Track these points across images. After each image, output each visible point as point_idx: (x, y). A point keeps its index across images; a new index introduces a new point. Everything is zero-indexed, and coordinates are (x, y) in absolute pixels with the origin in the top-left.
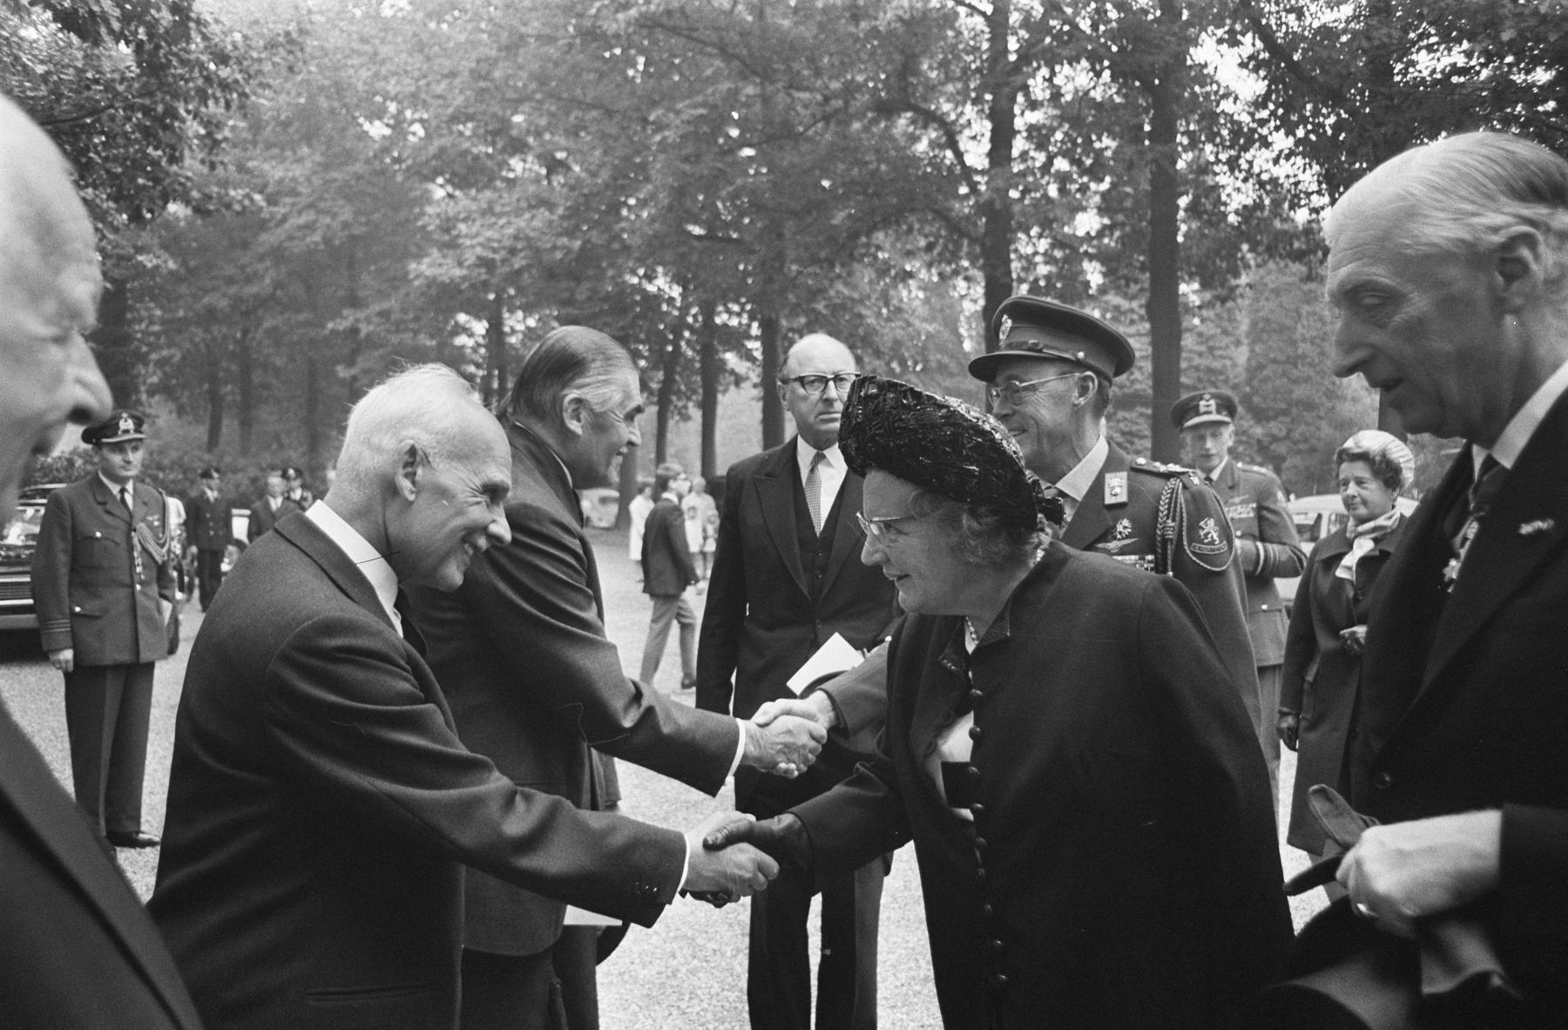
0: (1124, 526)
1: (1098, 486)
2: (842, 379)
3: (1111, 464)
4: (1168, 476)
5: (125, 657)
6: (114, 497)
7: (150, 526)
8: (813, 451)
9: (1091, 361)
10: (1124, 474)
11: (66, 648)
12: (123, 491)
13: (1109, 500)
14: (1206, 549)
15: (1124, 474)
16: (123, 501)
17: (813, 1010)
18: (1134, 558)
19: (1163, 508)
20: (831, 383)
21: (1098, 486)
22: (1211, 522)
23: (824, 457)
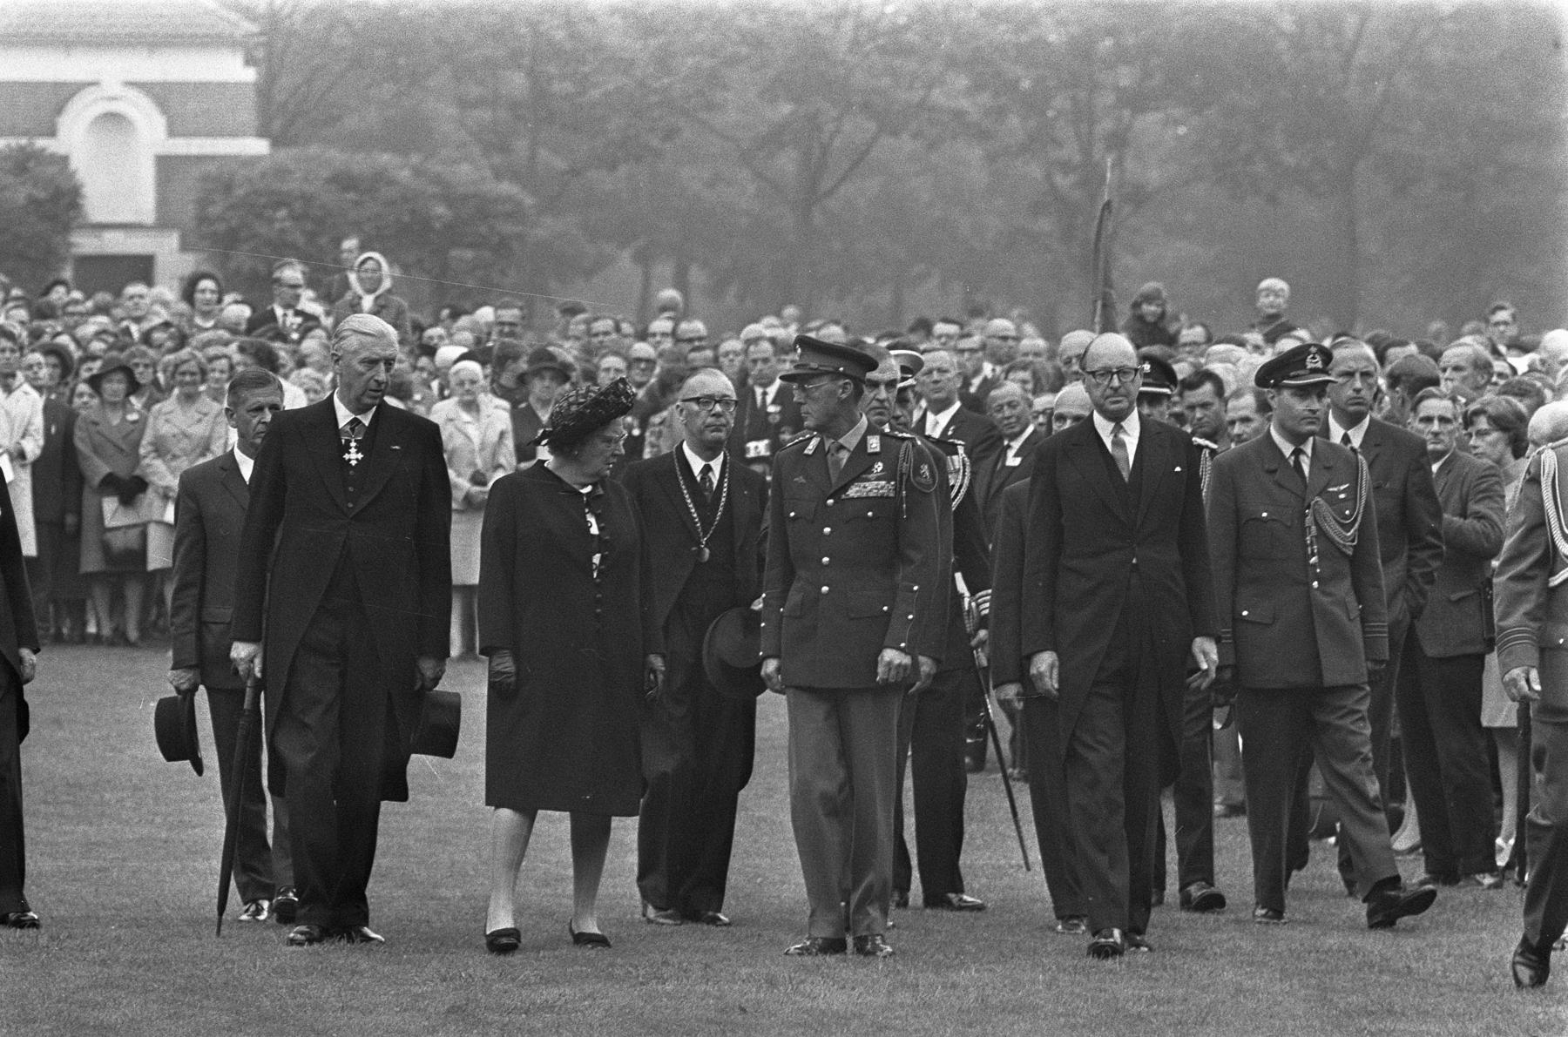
0: (879, 466)
1: (863, 443)
2: (1125, 373)
3: (871, 430)
4: (904, 439)
5: (1300, 677)
6: (1286, 460)
7: (1332, 500)
8: (1112, 425)
9: (849, 372)
10: (878, 437)
11: (1011, 682)
12: (1297, 452)
13: (870, 451)
14: (923, 481)
15: (878, 437)
16: (1298, 464)
17: (265, 771)
18: (884, 482)
19: (901, 456)
20: (1115, 376)
21: (863, 443)
22: (926, 467)
23: (1122, 427)
